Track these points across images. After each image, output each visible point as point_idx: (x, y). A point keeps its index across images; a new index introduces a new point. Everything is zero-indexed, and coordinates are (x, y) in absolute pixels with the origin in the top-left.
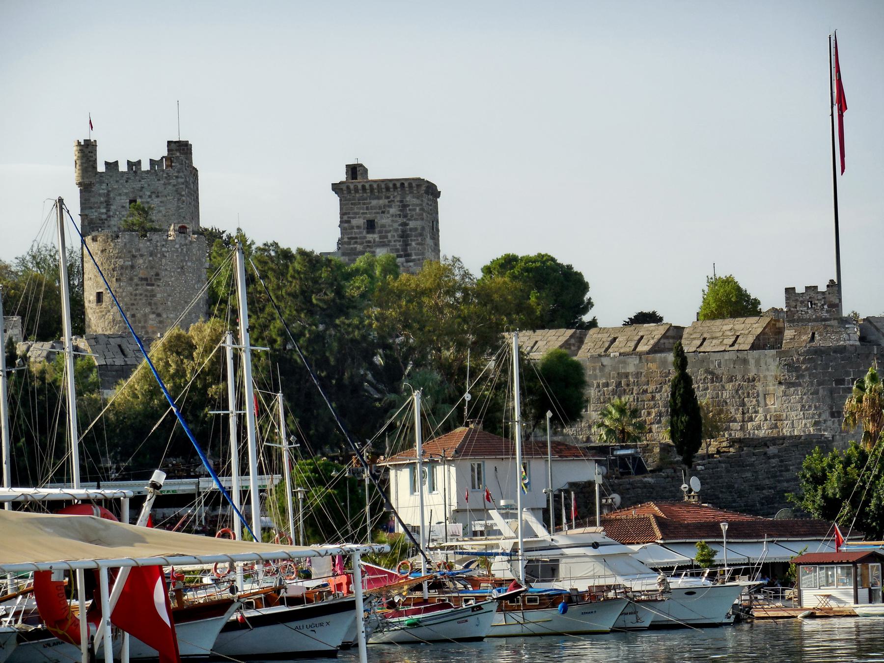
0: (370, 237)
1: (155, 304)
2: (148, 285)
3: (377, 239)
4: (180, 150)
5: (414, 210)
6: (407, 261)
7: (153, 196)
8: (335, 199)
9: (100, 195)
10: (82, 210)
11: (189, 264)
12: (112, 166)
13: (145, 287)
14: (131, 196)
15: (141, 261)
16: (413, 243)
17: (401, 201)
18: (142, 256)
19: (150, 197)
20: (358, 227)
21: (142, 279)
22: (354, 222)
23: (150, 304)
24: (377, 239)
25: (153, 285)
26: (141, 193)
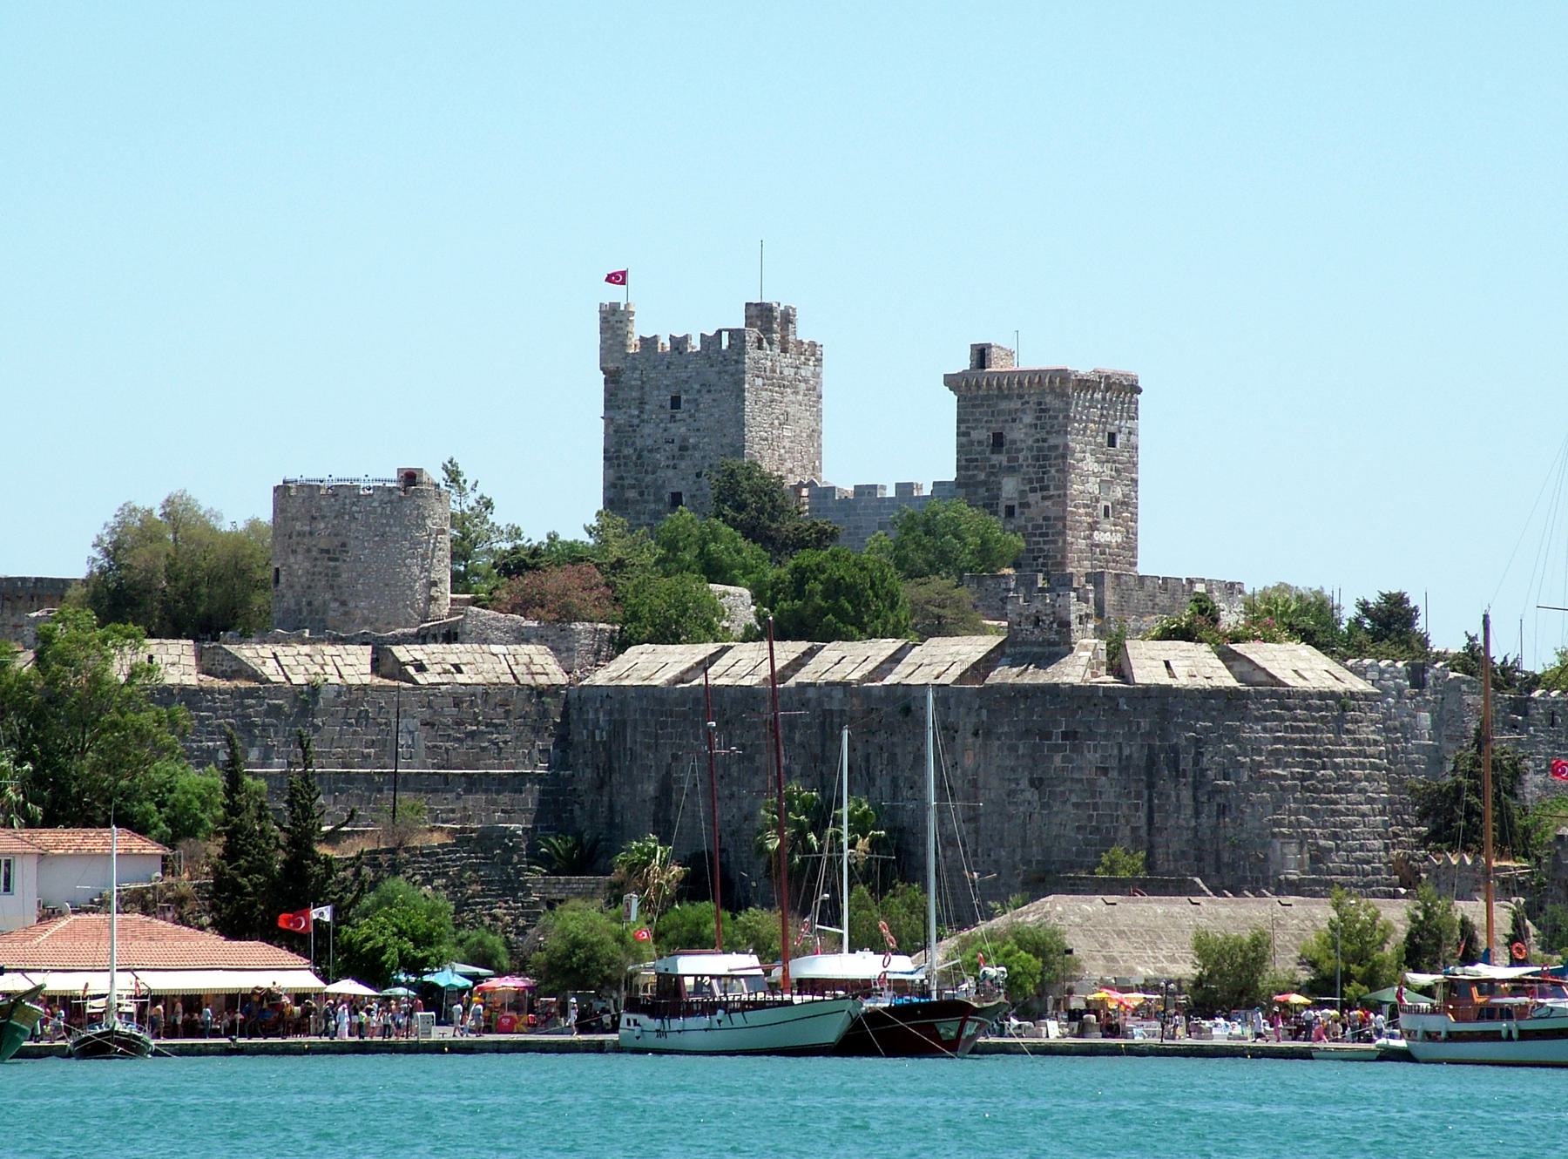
0: (996, 459)
1: (340, 587)
2: (330, 559)
3: (1005, 463)
4: (766, 319)
5: (1056, 417)
6: (1044, 498)
7: (704, 391)
8: (952, 399)
9: (631, 388)
10: (606, 408)
11: (395, 530)
12: (649, 343)
13: (326, 563)
14: (674, 391)
15: (322, 526)
16: (1053, 471)
17: (1039, 404)
18: (324, 517)
19: (699, 391)
20: (980, 443)
21: (322, 551)
22: (975, 435)
23: (332, 587)
24: (1005, 463)
25: (336, 560)
26: (687, 387)
